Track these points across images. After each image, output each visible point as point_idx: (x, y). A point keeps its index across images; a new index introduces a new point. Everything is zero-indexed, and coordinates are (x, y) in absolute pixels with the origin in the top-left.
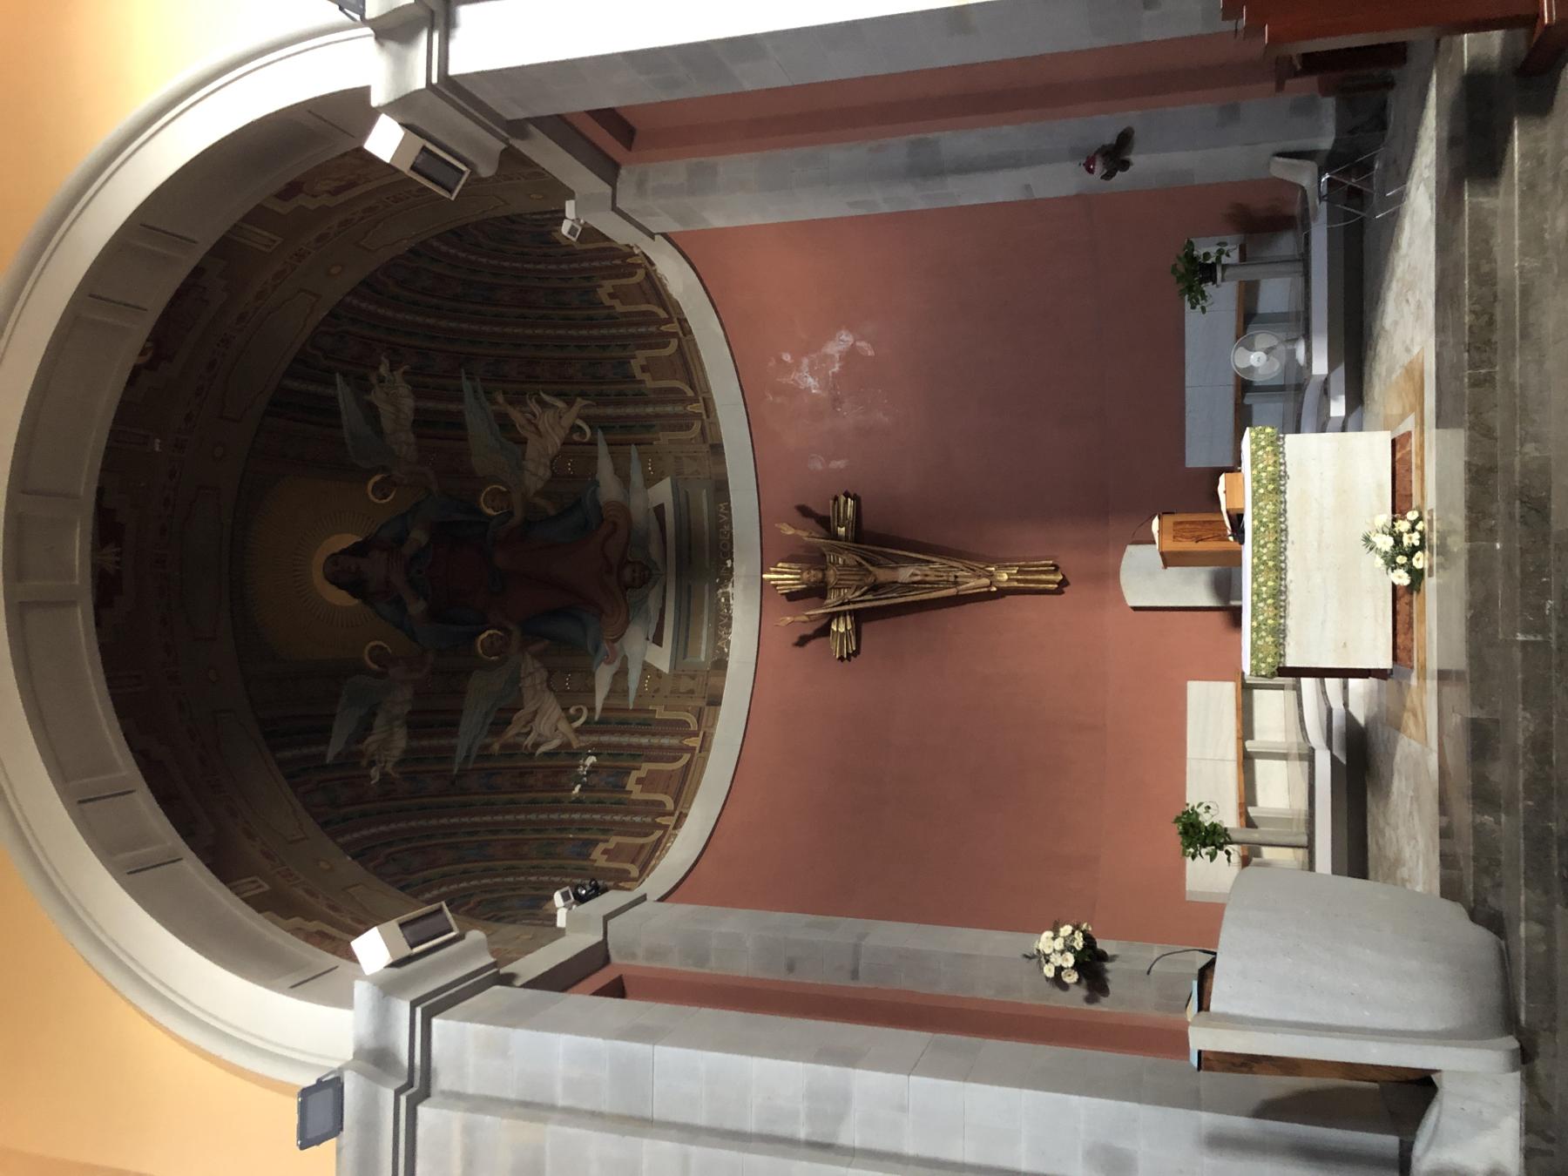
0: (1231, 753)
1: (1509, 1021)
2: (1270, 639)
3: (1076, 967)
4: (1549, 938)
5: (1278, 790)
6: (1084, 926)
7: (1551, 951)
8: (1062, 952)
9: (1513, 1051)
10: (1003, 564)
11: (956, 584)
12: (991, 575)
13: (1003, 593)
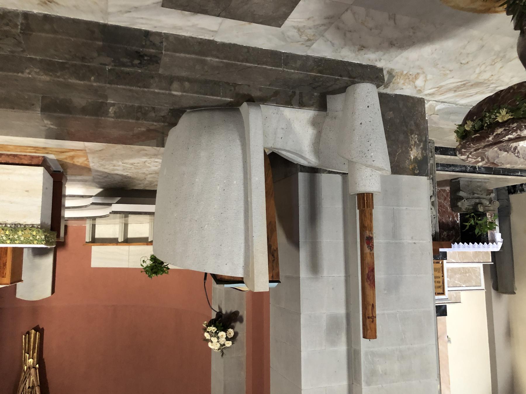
0: (125, 248)
1: (232, 108)
2: (20, 233)
3: (225, 330)
4: (181, 80)
5: (139, 228)
6: (205, 326)
7: (188, 80)
8: (218, 338)
9: (248, 105)
10: (23, 362)
11: (33, 387)
12: (29, 368)
13: (40, 360)
